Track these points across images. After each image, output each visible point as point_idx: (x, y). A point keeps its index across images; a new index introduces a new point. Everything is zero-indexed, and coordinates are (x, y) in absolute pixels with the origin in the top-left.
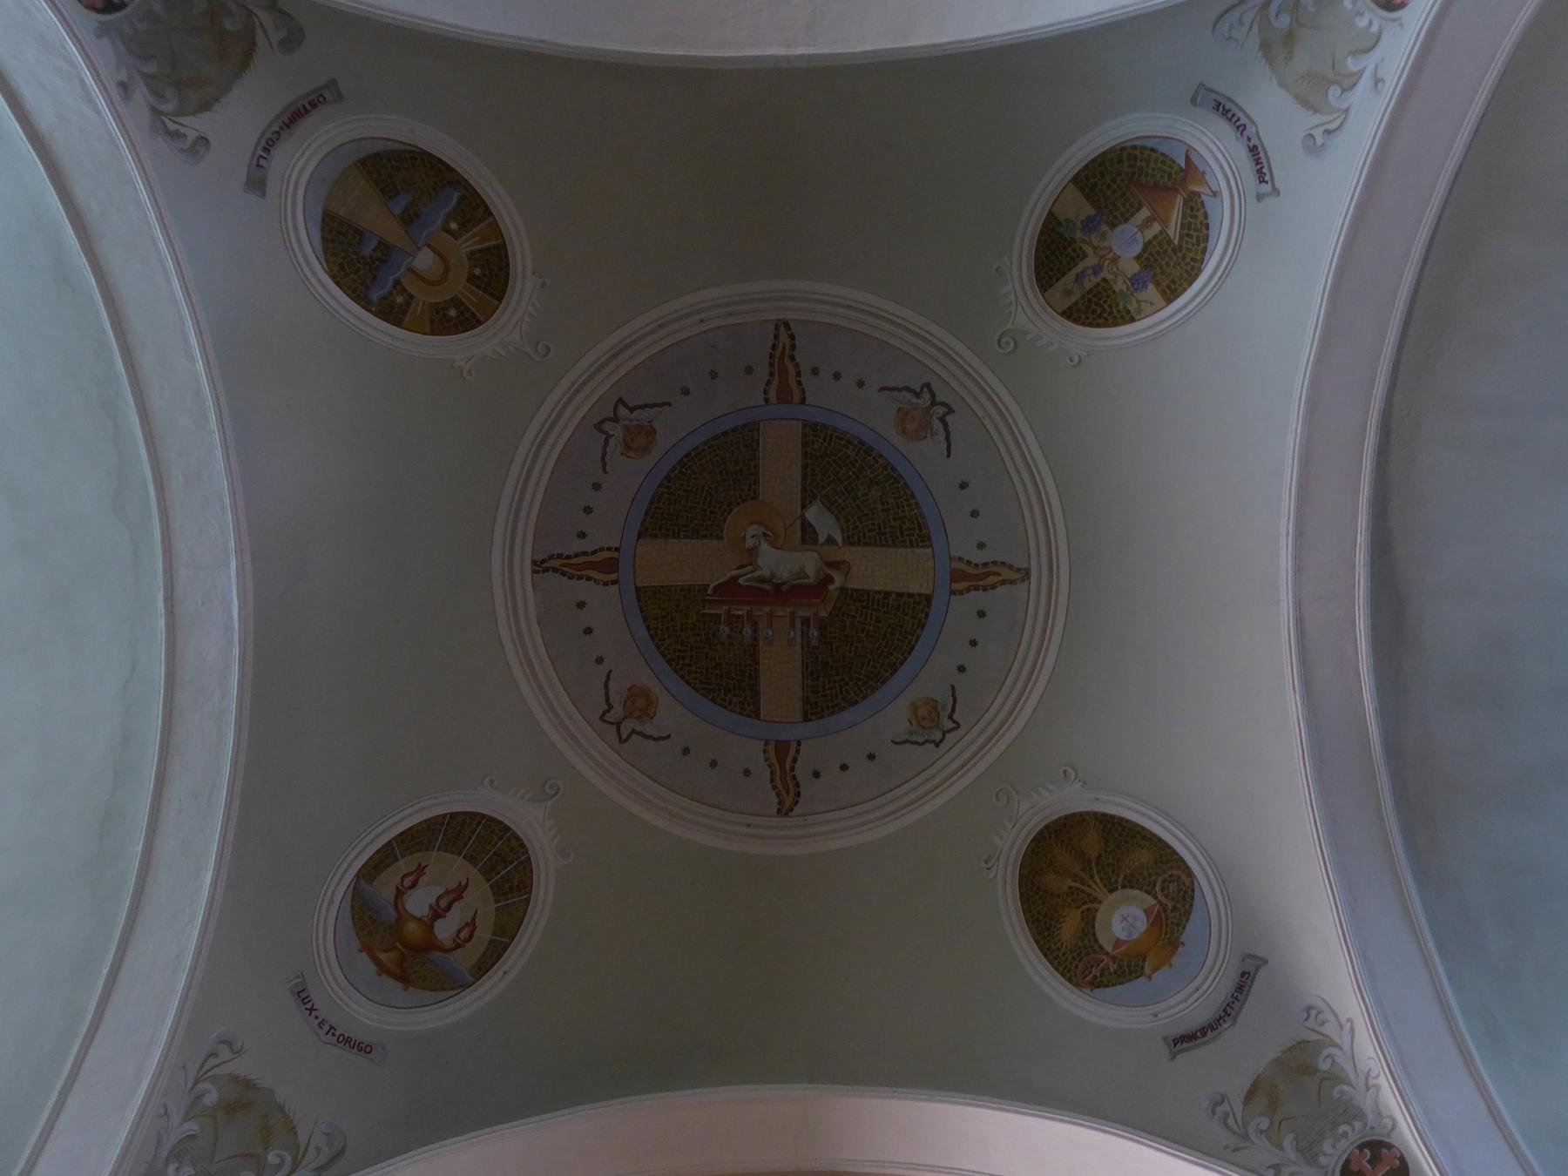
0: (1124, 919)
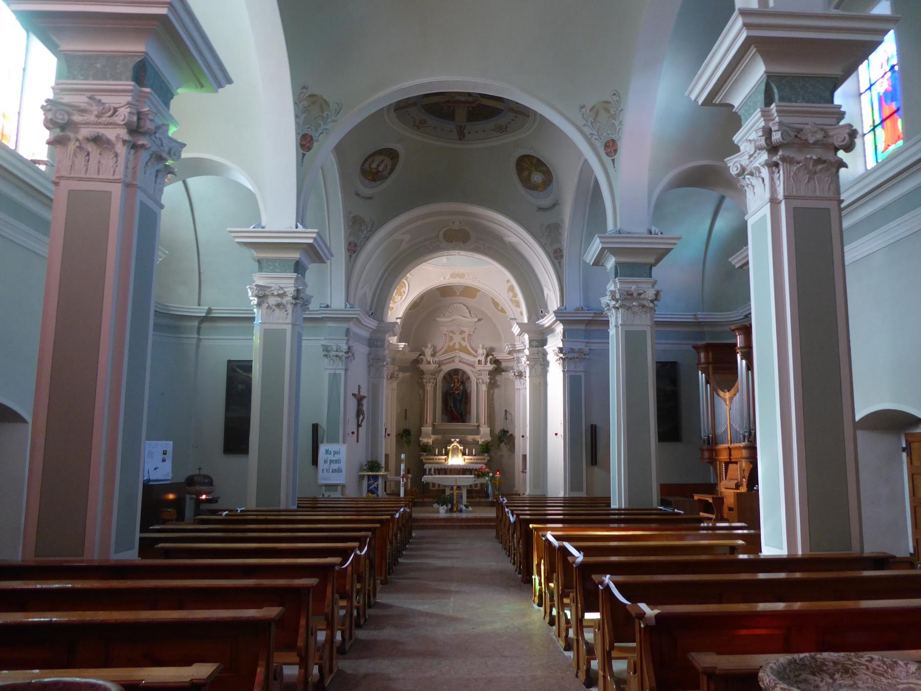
0: (537, 178)
